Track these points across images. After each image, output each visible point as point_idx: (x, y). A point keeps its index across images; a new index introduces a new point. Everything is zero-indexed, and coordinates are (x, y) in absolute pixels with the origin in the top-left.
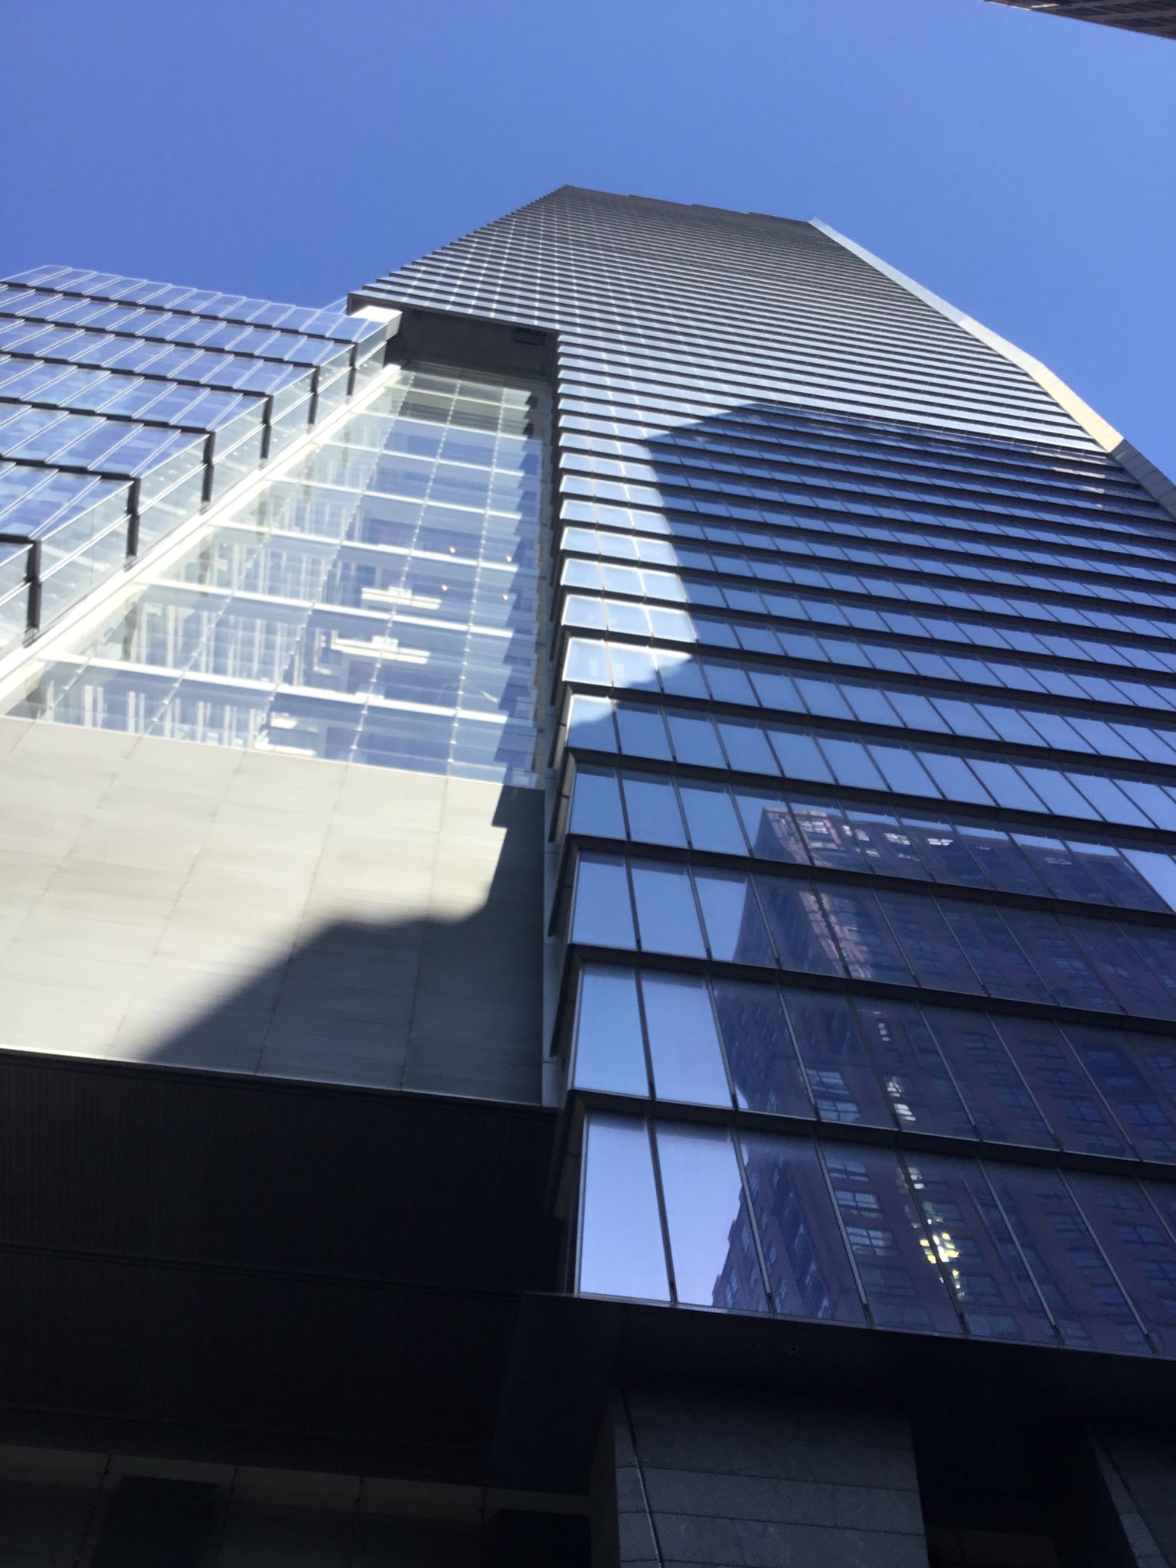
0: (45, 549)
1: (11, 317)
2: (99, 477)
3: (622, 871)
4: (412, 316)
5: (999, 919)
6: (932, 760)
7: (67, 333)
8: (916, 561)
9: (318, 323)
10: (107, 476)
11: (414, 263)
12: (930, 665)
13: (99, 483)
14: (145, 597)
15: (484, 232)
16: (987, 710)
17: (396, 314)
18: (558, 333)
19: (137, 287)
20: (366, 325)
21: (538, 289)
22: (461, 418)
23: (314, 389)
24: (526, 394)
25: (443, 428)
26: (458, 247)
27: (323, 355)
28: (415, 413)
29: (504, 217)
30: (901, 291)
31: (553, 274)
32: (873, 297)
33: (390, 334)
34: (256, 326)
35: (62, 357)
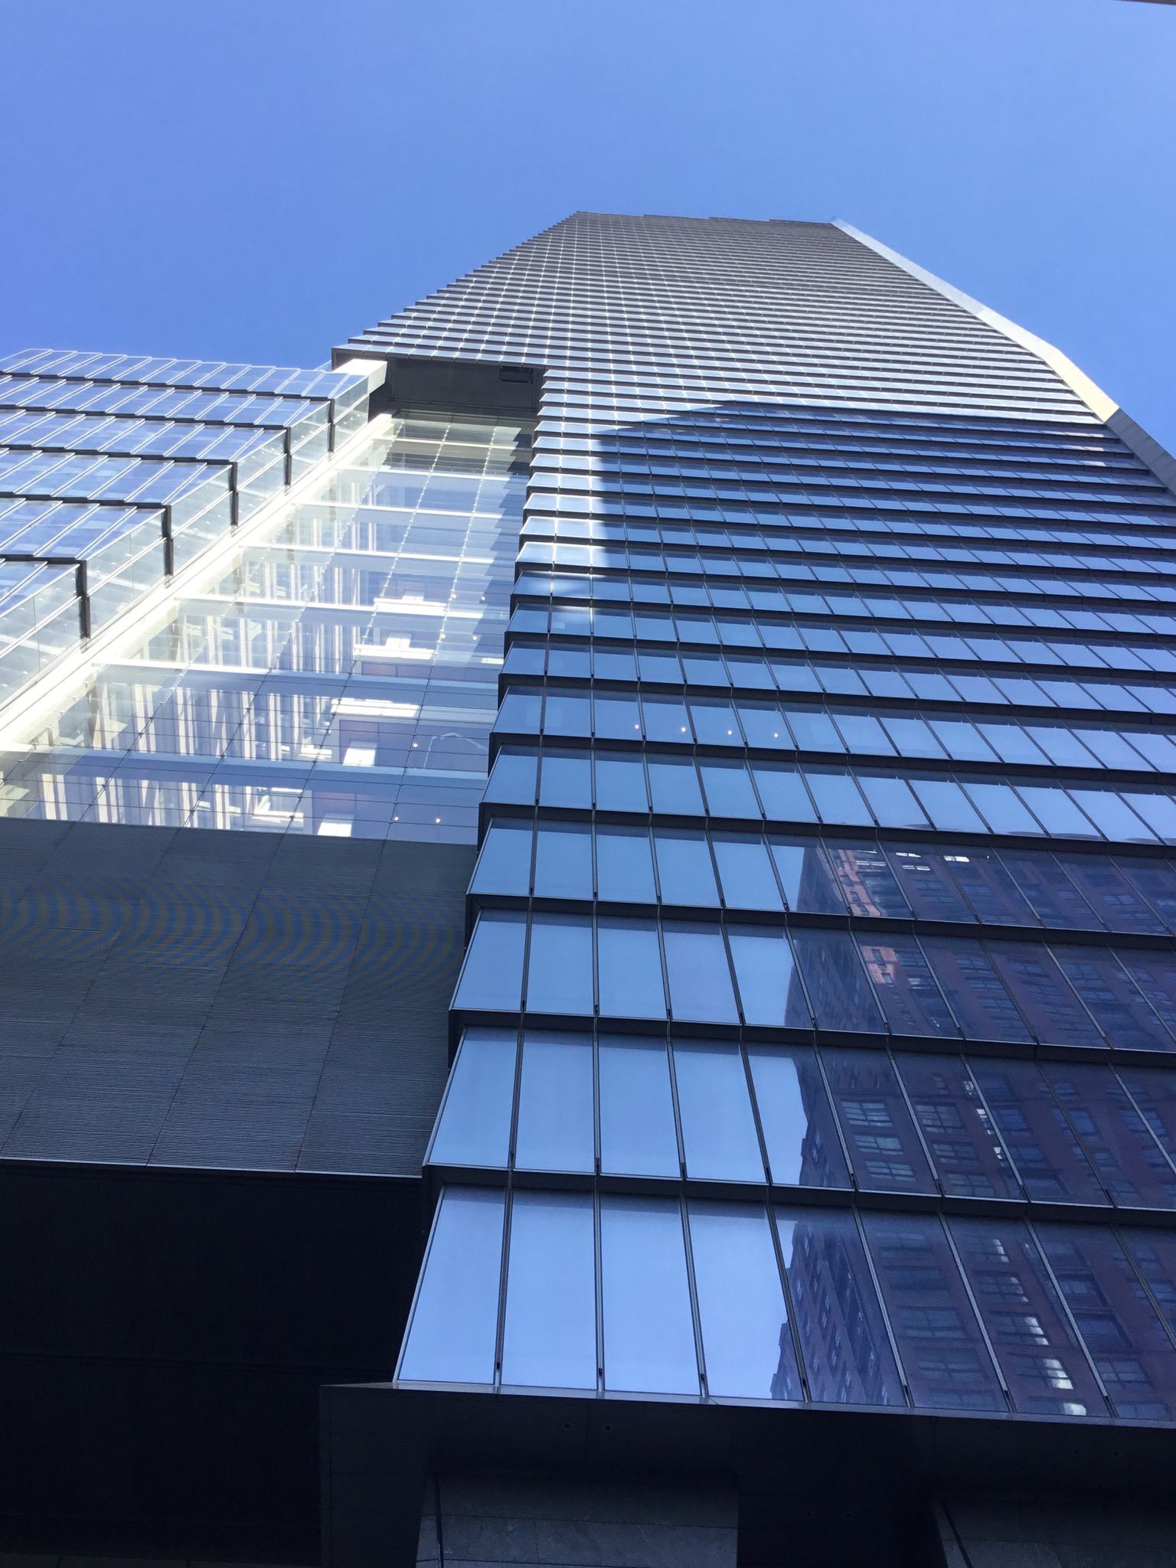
1: (12, 408)
2: (46, 562)
3: (718, 939)
4: (398, 365)
6: (1085, 797)
7: (158, 426)
8: (1000, 580)
9: (296, 382)
10: (52, 561)
11: (406, 310)
12: (1024, 692)
13: (47, 567)
14: (100, 678)
15: (483, 272)
16: (1136, 738)
17: (384, 363)
18: (545, 368)
19: (217, 372)
20: (345, 380)
22: (448, 463)
23: (287, 450)
24: (516, 431)
25: (426, 476)
26: (455, 288)
27: (296, 416)
30: (914, 282)
31: (586, 285)
32: (888, 296)
33: (372, 387)
34: (258, 394)
35: (126, 451)
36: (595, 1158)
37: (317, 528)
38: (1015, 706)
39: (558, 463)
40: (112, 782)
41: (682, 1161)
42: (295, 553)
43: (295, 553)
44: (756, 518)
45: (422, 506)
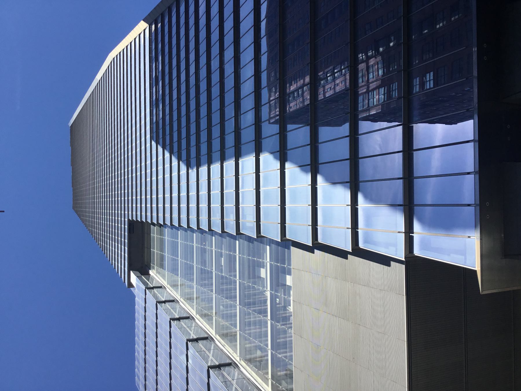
0: (209, 365)
5: (287, 77)
12: (229, 24)
18: (129, 220)
21: (106, 200)
26: (92, 232)
28: (164, 235)
29: (83, 224)
30: (90, 97)
33: (139, 274)
36: (398, 206)
37: (187, 290)
38: (234, 25)
39: (161, 197)
40: (278, 117)
41: (397, 179)
42: (197, 296)
43: (197, 296)
44: (175, 132)
45: (178, 257)
